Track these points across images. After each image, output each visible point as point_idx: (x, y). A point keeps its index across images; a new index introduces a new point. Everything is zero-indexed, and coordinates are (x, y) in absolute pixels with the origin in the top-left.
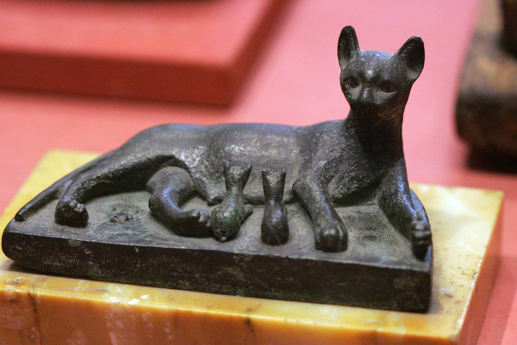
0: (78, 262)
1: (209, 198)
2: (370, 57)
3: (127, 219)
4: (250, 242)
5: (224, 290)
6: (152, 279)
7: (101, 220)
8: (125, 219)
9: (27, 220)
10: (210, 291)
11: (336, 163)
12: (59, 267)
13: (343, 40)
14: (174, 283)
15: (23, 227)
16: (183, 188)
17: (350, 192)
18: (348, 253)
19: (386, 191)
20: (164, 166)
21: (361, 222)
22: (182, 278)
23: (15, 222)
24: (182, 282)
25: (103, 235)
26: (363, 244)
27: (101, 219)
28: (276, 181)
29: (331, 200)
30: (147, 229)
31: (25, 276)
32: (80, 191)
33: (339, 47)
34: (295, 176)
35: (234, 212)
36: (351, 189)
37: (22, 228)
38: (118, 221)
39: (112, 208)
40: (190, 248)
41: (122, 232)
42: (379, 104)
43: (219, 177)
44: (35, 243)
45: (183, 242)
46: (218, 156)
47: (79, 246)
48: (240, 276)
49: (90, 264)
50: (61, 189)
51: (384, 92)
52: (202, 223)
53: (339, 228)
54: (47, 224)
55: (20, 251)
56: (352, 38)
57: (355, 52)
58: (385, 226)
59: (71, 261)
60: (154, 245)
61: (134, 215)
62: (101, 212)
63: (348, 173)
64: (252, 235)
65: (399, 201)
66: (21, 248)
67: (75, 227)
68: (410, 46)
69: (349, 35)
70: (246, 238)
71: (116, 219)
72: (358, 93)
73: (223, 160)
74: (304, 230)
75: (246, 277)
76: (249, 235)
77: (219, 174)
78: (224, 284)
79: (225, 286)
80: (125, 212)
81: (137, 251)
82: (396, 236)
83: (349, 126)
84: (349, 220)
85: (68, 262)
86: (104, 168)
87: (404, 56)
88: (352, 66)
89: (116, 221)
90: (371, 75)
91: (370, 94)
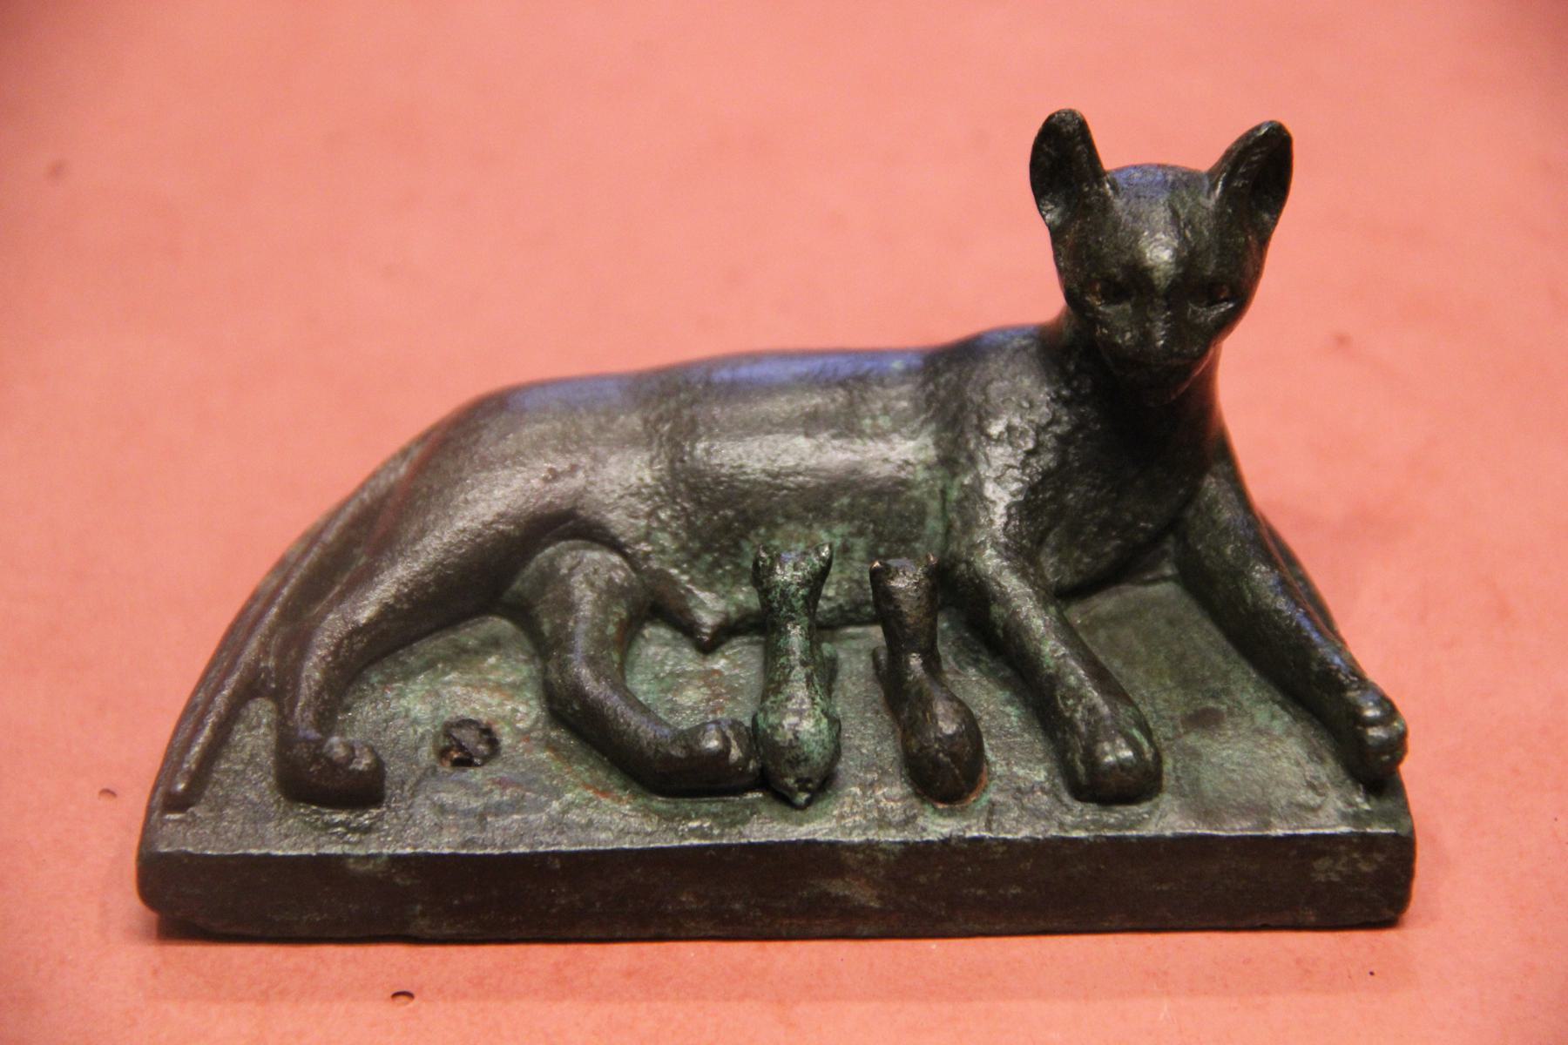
13: (1049, 146)
43: (717, 564)
48: (863, 894)
52: (736, 765)
68: (1255, 155)
83: (1072, 367)
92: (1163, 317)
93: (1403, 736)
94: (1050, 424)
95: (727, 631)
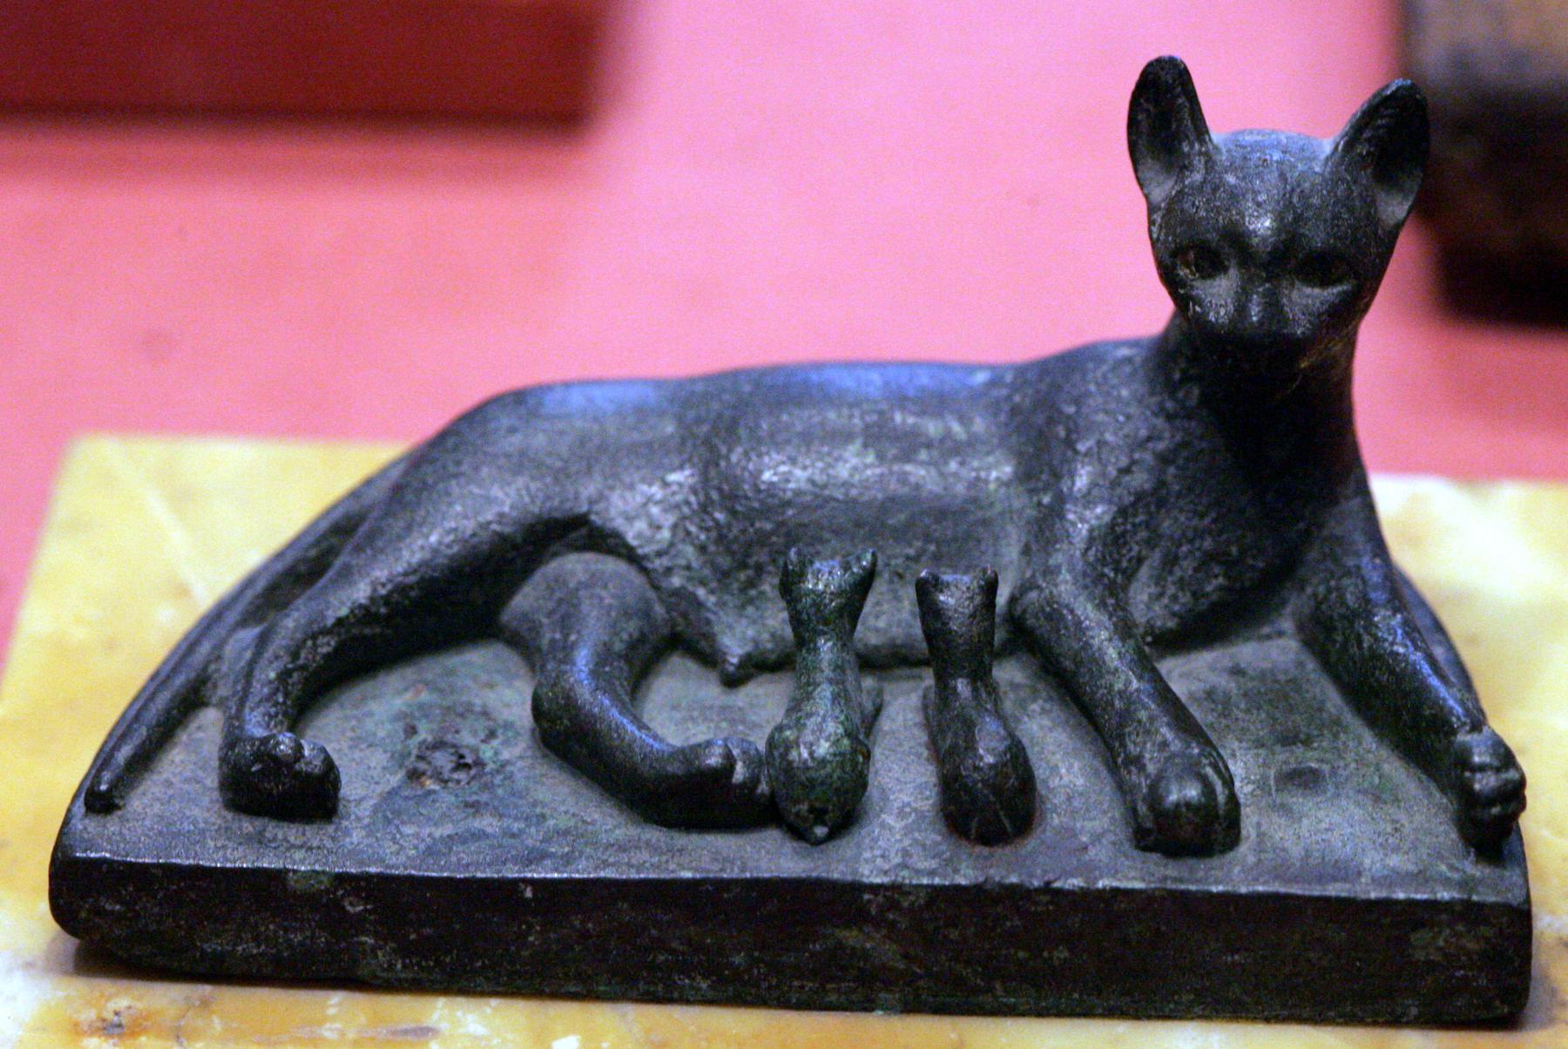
0: (321, 937)
1: (725, 661)
2: (1247, 159)
3: (461, 765)
4: (907, 831)
5: (833, 998)
6: (580, 978)
7: (377, 779)
8: (453, 765)
9: (125, 805)
10: (784, 1004)
11: (1150, 514)
12: (253, 956)
13: (1147, 100)
14: (656, 984)
15: (121, 833)
16: (636, 635)
17: (1203, 605)
18: (1245, 850)
19: (1326, 598)
20: (555, 555)
21: (1255, 712)
22: (687, 969)
23: (86, 815)
24: (687, 981)
25: (402, 846)
26: (1285, 809)
27: (375, 773)
28: (967, 611)
29: (1143, 638)
30: (544, 805)
31: (136, 993)
32: (290, 681)
33: (1132, 124)
34: (1012, 562)
35: (846, 742)
36: (1206, 595)
37: (118, 838)
38: (429, 773)
39: (400, 726)
40: (711, 875)
41: (461, 829)
42: (1303, 333)
44: (167, 889)
45: (681, 851)
46: (739, 508)
47: (327, 889)
48: (888, 952)
49: (366, 942)
50: (217, 671)
51: (1313, 287)
52: (743, 785)
53: (1209, 771)
54: (196, 812)
55: (118, 917)
56: (1180, 101)
57: (1197, 146)
58: (1337, 724)
59: (297, 938)
60: (581, 871)
61: (483, 747)
62: (370, 746)
63: (1191, 541)
64: (909, 804)
65: (1386, 645)
66: (118, 907)
67: (300, 822)
68: (1382, 117)
69: (1171, 88)
70: (889, 819)
71: (422, 766)
72: (1229, 301)
73: (758, 525)
74: (1076, 765)
75: (906, 956)
76: (896, 805)
77: (750, 572)
78: (832, 979)
79: (833, 986)
80: (449, 738)
81: (529, 894)
82: (1386, 767)
83: (1177, 376)
84: (1213, 710)
85: (286, 941)
86: (352, 584)
87: (1364, 153)
88: (1197, 203)
89: (424, 773)
90: (1270, 240)
91: (1273, 306)
92: (1261, 289)
93: (1521, 783)
94: (1149, 439)
95: (757, 666)
